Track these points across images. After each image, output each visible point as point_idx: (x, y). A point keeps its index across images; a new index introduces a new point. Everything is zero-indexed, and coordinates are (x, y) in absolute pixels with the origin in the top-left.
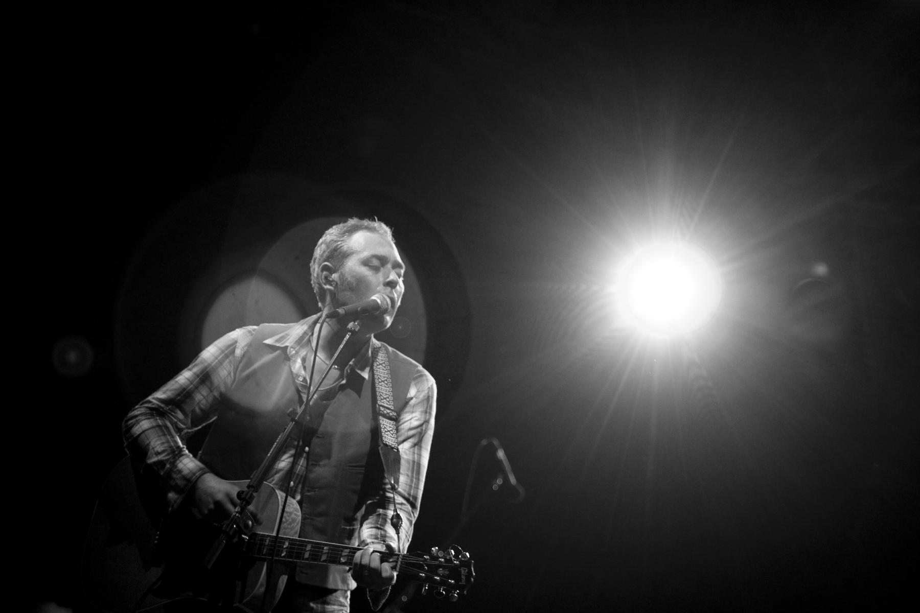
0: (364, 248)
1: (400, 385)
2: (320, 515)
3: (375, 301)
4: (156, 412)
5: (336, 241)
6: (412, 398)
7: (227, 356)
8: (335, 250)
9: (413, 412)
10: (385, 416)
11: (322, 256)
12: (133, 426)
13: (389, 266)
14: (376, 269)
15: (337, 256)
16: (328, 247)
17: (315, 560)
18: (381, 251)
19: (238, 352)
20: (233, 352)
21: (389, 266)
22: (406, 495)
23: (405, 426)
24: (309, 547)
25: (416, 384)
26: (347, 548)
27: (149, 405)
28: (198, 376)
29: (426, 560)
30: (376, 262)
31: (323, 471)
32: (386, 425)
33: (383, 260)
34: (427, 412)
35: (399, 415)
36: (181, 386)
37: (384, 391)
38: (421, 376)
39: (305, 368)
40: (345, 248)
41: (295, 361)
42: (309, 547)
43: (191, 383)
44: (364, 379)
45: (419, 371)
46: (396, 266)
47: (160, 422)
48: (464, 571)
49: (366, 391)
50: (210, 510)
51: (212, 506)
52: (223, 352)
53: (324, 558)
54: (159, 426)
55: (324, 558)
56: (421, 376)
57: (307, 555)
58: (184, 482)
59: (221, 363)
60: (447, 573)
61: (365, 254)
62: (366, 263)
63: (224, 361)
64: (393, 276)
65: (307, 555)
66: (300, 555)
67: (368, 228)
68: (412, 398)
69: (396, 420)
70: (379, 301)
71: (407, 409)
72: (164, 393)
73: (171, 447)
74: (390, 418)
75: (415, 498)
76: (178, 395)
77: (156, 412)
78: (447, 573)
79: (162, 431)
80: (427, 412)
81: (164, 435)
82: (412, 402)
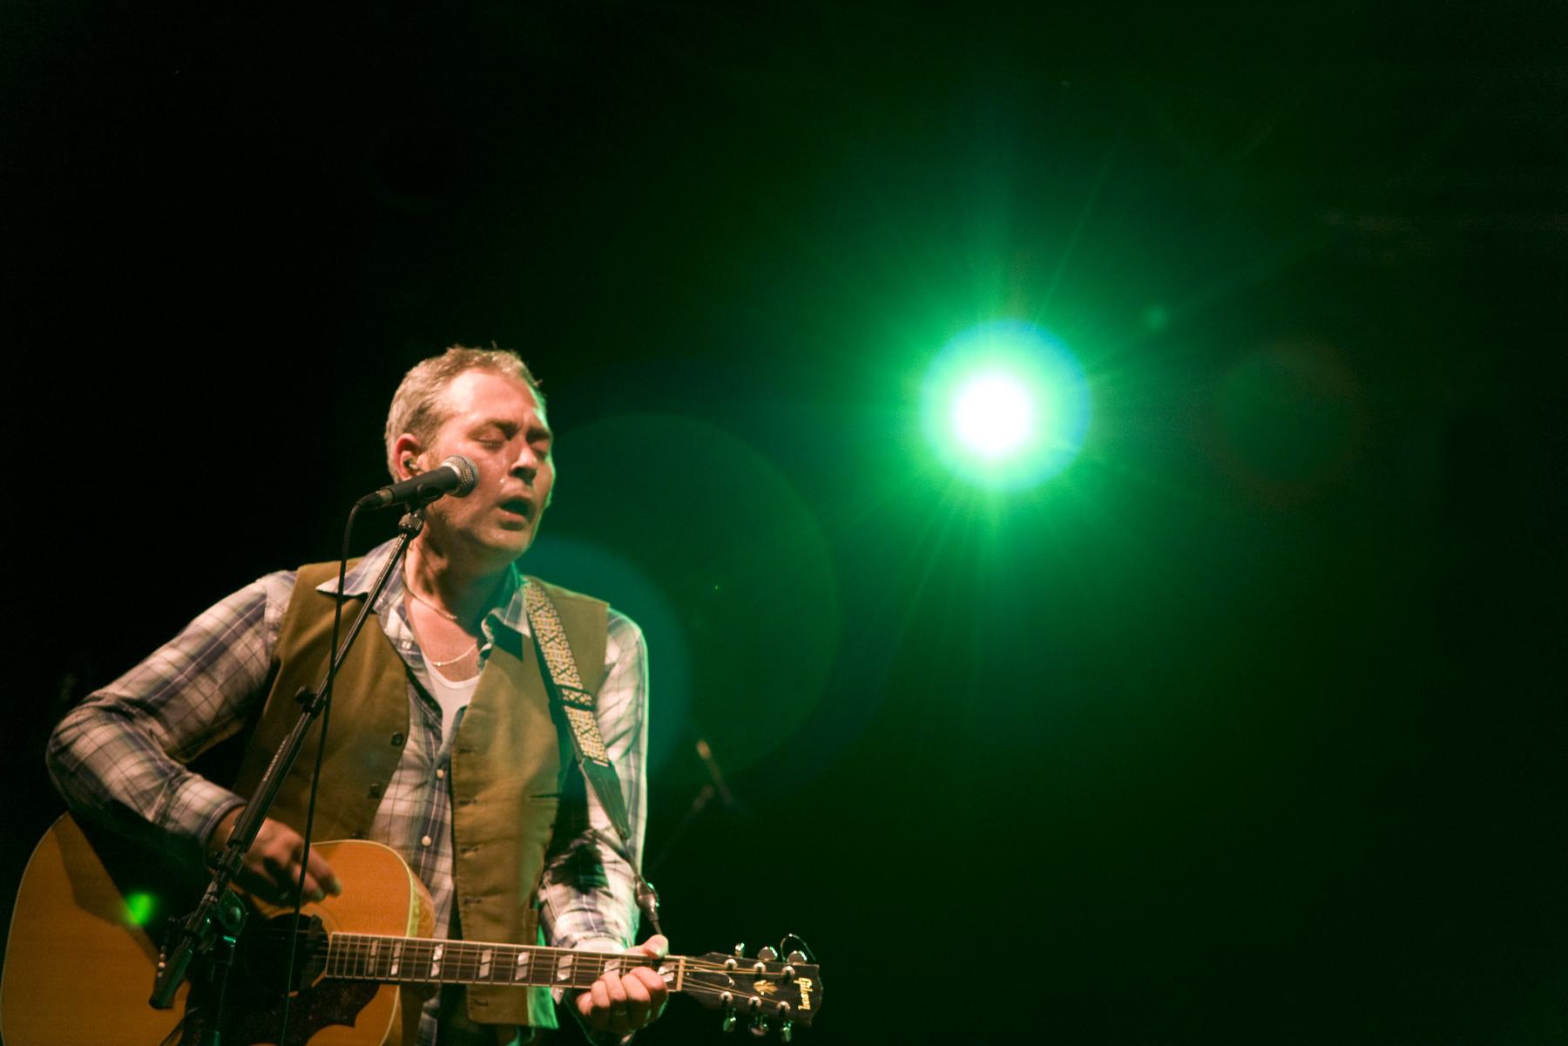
0: (464, 406)
2: (488, 893)
3: (449, 469)
4: (119, 711)
5: (422, 394)
6: (613, 665)
7: (249, 624)
8: (422, 411)
9: (618, 690)
10: (573, 704)
11: (399, 420)
12: (73, 742)
13: (521, 437)
14: (494, 447)
15: (425, 420)
16: (409, 405)
17: (505, 978)
18: (506, 410)
19: (271, 614)
20: (260, 615)
21: (521, 437)
23: (609, 717)
24: (486, 958)
25: (615, 638)
26: (565, 954)
27: (101, 703)
28: (193, 658)
29: (730, 966)
30: (495, 434)
31: (486, 812)
32: (578, 718)
33: (508, 430)
35: (595, 699)
36: (160, 676)
37: (558, 656)
38: (619, 623)
39: (408, 625)
40: (438, 407)
41: (386, 618)
42: (486, 958)
43: (181, 670)
44: (520, 635)
45: (611, 616)
46: (534, 435)
47: (128, 729)
52: (241, 615)
53: (521, 974)
54: (128, 735)
55: (521, 974)
56: (619, 623)
57: (484, 971)
58: (199, 822)
60: (773, 989)
61: (476, 418)
62: (475, 435)
64: (526, 458)
65: (484, 971)
67: (487, 365)
68: (613, 665)
69: (593, 708)
70: (456, 470)
71: (609, 684)
72: (125, 687)
73: (158, 768)
74: (582, 707)
76: (156, 692)
77: (119, 711)
78: (773, 989)
79: (137, 743)
81: (142, 749)
82: (615, 672)
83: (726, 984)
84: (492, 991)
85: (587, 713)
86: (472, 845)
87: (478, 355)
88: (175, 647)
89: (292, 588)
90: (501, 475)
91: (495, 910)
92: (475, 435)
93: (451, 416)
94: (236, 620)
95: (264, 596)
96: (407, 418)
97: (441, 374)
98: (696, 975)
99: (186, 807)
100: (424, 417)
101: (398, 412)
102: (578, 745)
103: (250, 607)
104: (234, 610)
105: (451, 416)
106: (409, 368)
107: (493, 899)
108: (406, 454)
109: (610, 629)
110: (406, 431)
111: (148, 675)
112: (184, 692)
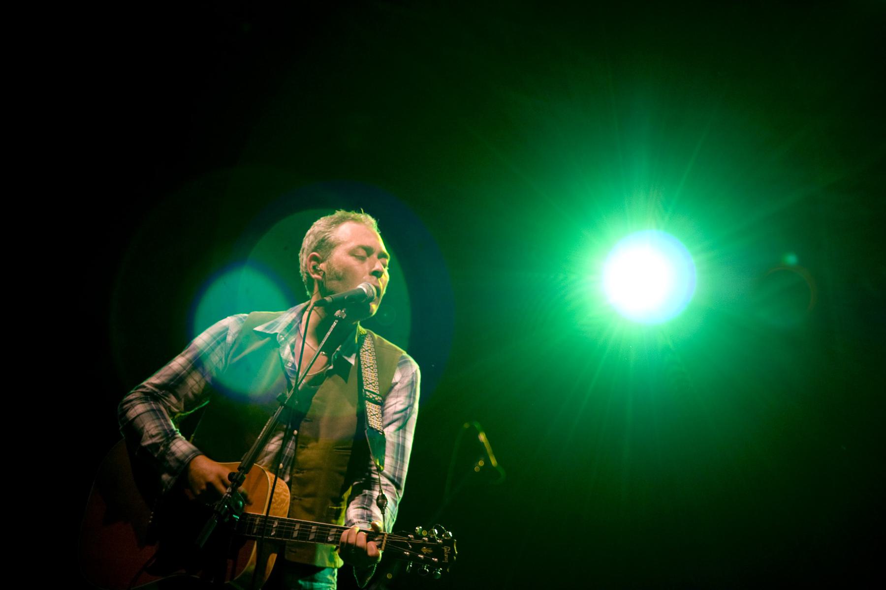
1: (385, 369)
5: (324, 232)
7: (218, 343)
8: (323, 240)
9: (397, 397)
10: (370, 400)
11: (310, 246)
13: (375, 256)
14: (362, 259)
15: (324, 246)
16: (316, 238)
19: (230, 339)
20: (225, 339)
21: (375, 256)
22: (391, 477)
23: (390, 410)
27: (144, 390)
30: (362, 253)
31: (312, 454)
32: (372, 409)
33: (369, 251)
34: (411, 396)
35: (384, 399)
37: (370, 376)
42: (297, 527)
45: (403, 357)
46: (382, 256)
48: (446, 549)
49: (353, 378)
50: (202, 491)
51: (204, 487)
53: (312, 537)
54: (153, 410)
55: (312, 537)
57: (295, 534)
59: (213, 349)
60: (430, 551)
61: (352, 245)
62: (352, 253)
63: (216, 348)
64: (378, 266)
65: (295, 534)
66: (289, 535)
69: (382, 404)
70: (365, 290)
71: (392, 394)
72: (158, 378)
73: (164, 430)
74: (376, 403)
75: (400, 479)
76: (172, 380)
78: (430, 551)
79: (157, 415)
80: (411, 396)
81: (158, 419)
82: (397, 387)
83: (408, 548)
84: (300, 545)
85: (377, 406)
86: (301, 470)
87: (353, 214)
88: (183, 356)
89: (241, 325)
90: (365, 274)
91: (308, 505)
92: (352, 253)
93: (339, 244)
94: (212, 341)
95: (227, 329)
96: (314, 244)
97: (333, 223)
98: (393, 543)
99: (173, 454)
100: (324, 244)
101: (308, 241)
102: (368, 420)
103: (221, 333)
104: (212, 336)
105: (339, 244)
106: (315, 220)
107: (307, 499)
108: (313, 263)
109: (399, 365)
110: (313, 251)
111: (169, 372)
112: (300, 458)
